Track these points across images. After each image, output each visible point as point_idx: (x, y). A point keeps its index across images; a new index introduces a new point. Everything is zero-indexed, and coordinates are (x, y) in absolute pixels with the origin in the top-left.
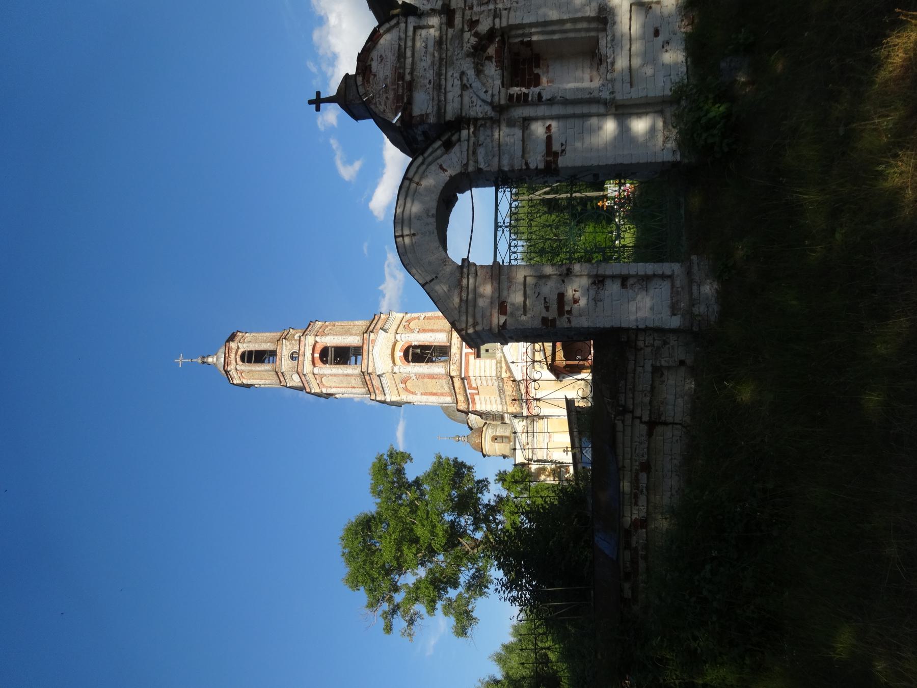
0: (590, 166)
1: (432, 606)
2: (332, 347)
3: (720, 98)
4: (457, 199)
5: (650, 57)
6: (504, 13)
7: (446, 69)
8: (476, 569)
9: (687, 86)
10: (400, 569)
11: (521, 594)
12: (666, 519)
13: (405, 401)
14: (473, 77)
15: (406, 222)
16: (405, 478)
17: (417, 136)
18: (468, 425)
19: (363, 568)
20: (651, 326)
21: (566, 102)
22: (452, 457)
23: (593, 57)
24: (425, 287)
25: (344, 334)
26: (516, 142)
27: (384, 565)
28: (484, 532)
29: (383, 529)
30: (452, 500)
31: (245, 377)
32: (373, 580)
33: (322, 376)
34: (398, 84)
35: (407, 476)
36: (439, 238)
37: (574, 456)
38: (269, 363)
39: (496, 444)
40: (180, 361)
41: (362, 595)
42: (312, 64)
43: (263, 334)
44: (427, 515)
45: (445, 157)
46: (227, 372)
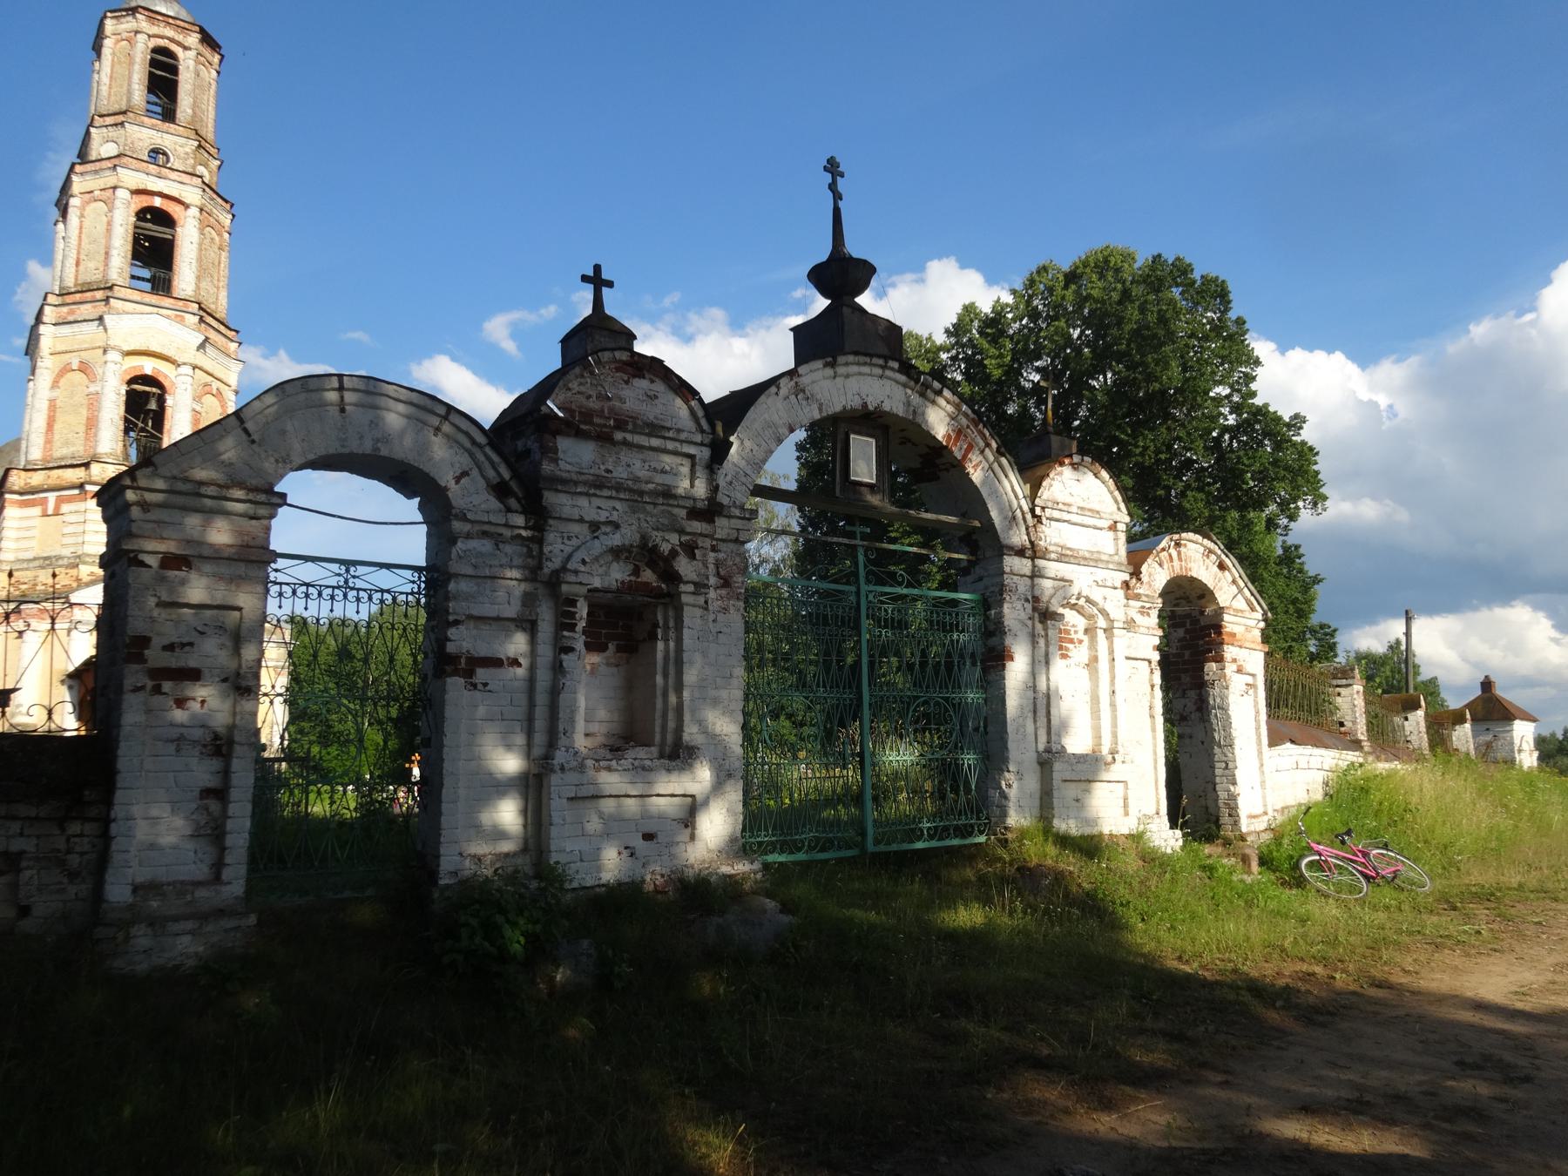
2: (173, 236)
3: (532, 940)
4: (409, 496)
5: (614, 827)
6: (701, 600)
9: (562, 889)
13: (39, 364)
14: (609, 543)
15: (370, 399)
20: (114, 847)
21: (555, 692)
23: (624, 738)
24: (233, 418)
26: (496, 607)
31: (118, 46)
33: (110, 204)
34: (609, 418)
36: (333, 455)
38: (148, 102)
45: (482, 483)
46: (133, 11)
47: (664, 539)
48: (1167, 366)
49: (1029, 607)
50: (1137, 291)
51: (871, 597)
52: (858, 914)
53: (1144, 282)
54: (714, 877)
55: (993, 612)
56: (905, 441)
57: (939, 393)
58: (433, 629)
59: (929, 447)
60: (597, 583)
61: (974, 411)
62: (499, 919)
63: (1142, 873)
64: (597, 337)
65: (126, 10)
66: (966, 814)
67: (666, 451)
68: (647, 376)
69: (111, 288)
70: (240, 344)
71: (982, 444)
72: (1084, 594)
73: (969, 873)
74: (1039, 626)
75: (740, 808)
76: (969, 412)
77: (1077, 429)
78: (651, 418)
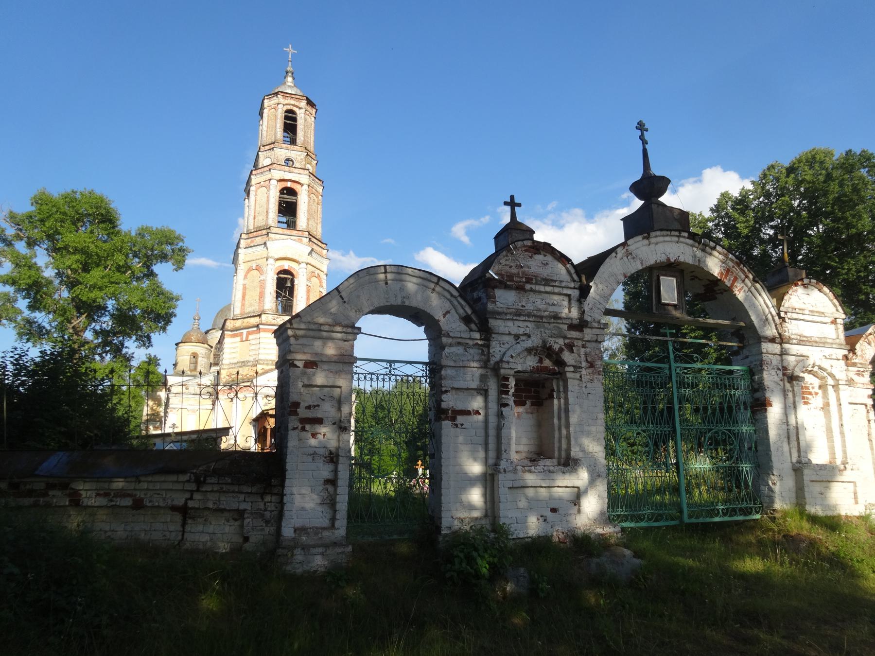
0: (441, 451)
1: (7, 281)
3: (493, 567)
4: (419, 325)
5: (534, 504)
6: (578, 376)
7: (534, 321)
8: (50, 331)
9: (507, 538)
10: (55, 250)
11: (8, 375)
12: (78, 526)
13: (238, 268)
14: (525, 346)
15: (398, 277)
16: (157, 262)
17: (477, 292)
18: (211, 330)
19: (57, 211)
20: (285, 508)
21: (499, 428)
22: (177, 311)
25: (309, 214)
26: (466, 382)
27: (59, 234)
28: (92, 341)
29: (100, 236)
30: (130, 309)
32: (42, 221)
33: (268, 188)
34: (522, 277)
35: (159, 264)
37: (169, 435)
38: (284, 137)
39: (189, 357)
40: (290, 50)
41: (25, 207)
42: (554, 206)
43: (313, 134)
44: (114, 283)
45: (457, 316)
46: (277, 94)
47: (555, 342)
48: (860, 218)
49: (780, 373)
50: (836, 174)
51: (678, 370)
52: (681, 560)
53: (841, 167)
54: (593, 535)
55: (756, 377)
56: (694, 278)
57: (714, 248)
58: (433, 395)
59: (709, 280)
60: (519, 368)
61: (737, 257)
62: (475, 554)
63: (870, 541)
64: (514, 234)
65: (273, 94)
66: (746, 501)
67: (554, 293)
68: (542, 253)
69: (269, 228)
70: (328, 250)
71: (743, 276)
72: (817, 364)
73: (751, 538)
74: (788, 385)
75: (606, 495)
76: (734, 258)
77: (800, 261)
78: (545, 276)
